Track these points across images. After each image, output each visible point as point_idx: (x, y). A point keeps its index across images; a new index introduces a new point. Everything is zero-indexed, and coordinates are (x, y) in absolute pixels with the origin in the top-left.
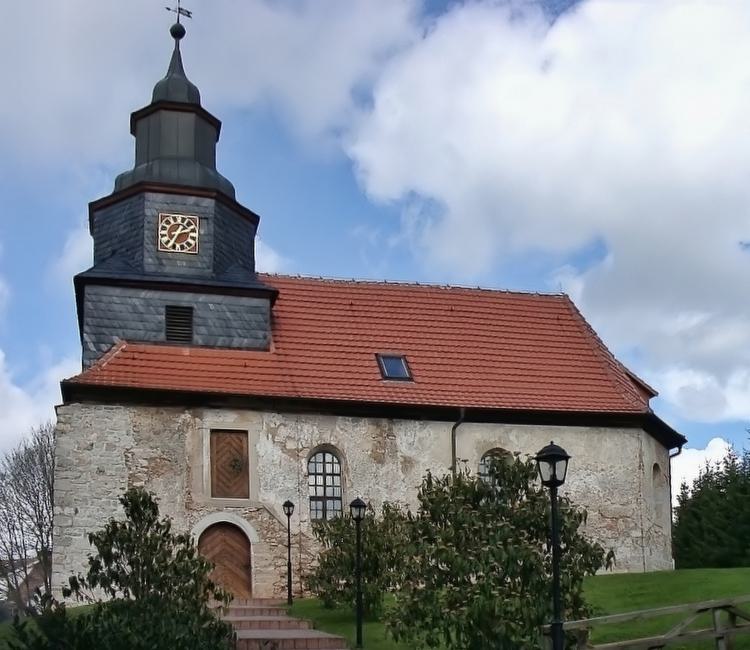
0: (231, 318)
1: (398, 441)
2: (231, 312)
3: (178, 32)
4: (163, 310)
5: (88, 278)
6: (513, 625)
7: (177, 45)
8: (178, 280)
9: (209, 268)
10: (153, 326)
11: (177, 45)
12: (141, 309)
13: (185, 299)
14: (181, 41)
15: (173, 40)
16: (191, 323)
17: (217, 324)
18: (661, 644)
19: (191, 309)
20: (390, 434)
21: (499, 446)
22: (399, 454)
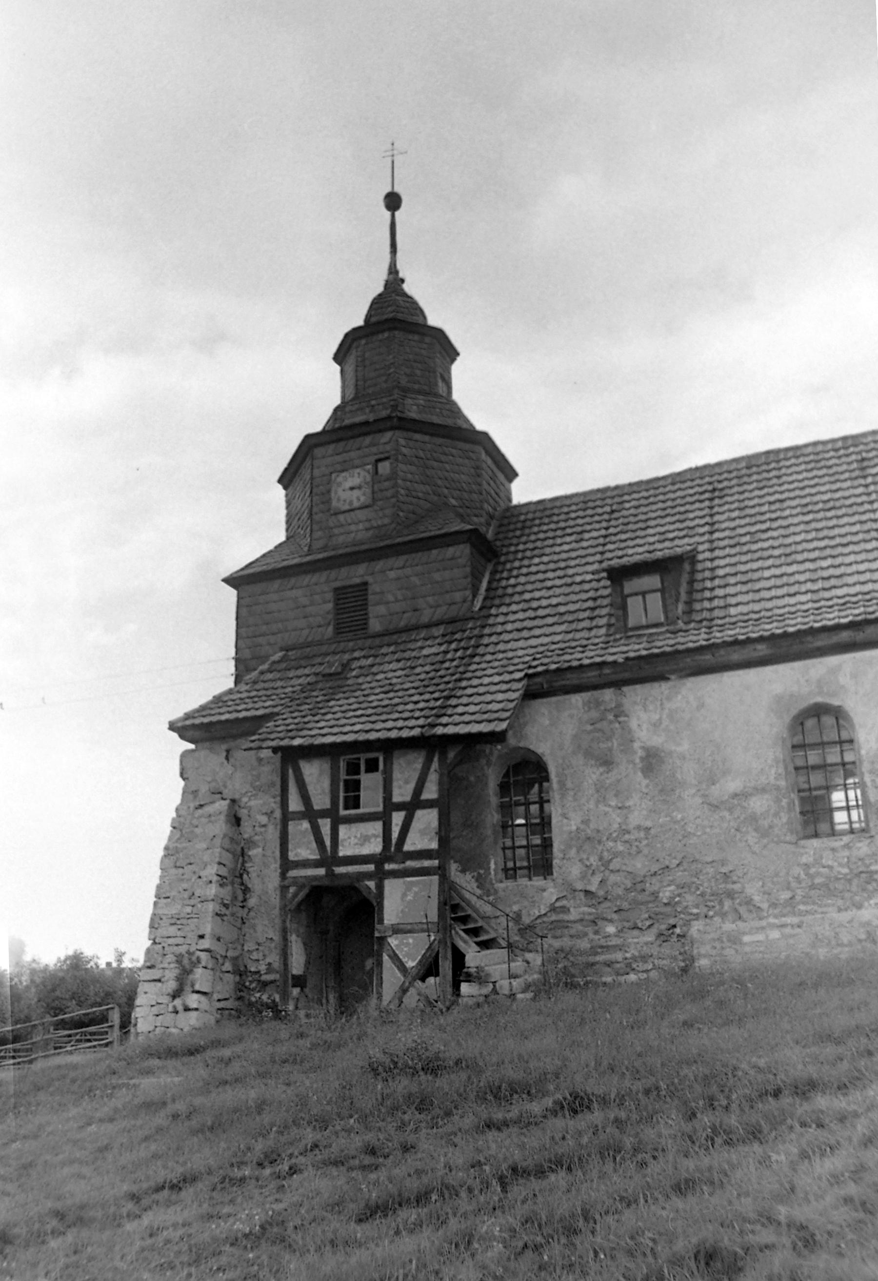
0: (418, 583)
1: (633, 724)
2: (416, 575)
3: (393, 202)
4: (330, 596)
5: (249, 576)
6: (670, 1122)
7: (393, 216)
8: (348, 550)
9: (466, 577)
10: (319, 620)
11: (393, 216)
12: (304, 601)
13: (357, 574)
14: (397, 213)
15: (388, 214)
16: (366, 604)
17: (400, 597)
18: (234, 820)
19: (366, 584)
20: (619, 713)
21: (819, 699)
22: (636, 745)
